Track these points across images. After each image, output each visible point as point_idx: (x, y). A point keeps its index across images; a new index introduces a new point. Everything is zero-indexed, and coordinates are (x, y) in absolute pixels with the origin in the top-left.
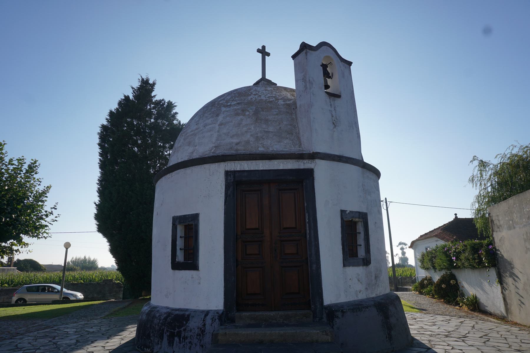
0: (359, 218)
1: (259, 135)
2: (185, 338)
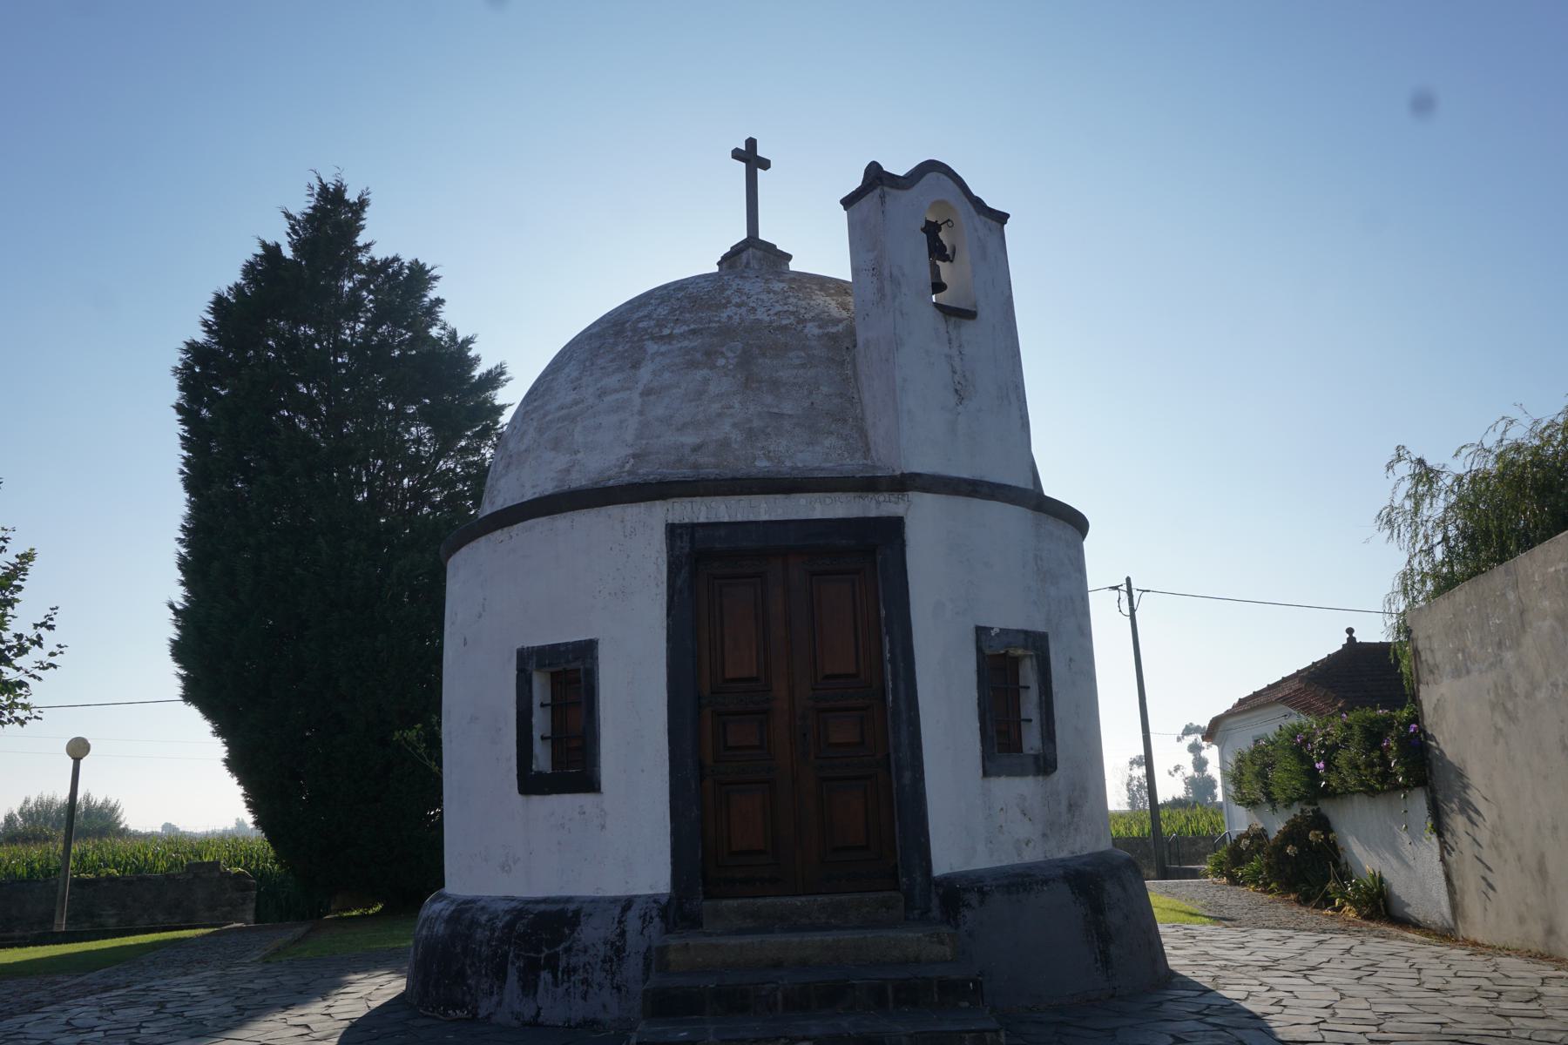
0: (1026, 648)
1: (756, 423)
2: (570, 971)
